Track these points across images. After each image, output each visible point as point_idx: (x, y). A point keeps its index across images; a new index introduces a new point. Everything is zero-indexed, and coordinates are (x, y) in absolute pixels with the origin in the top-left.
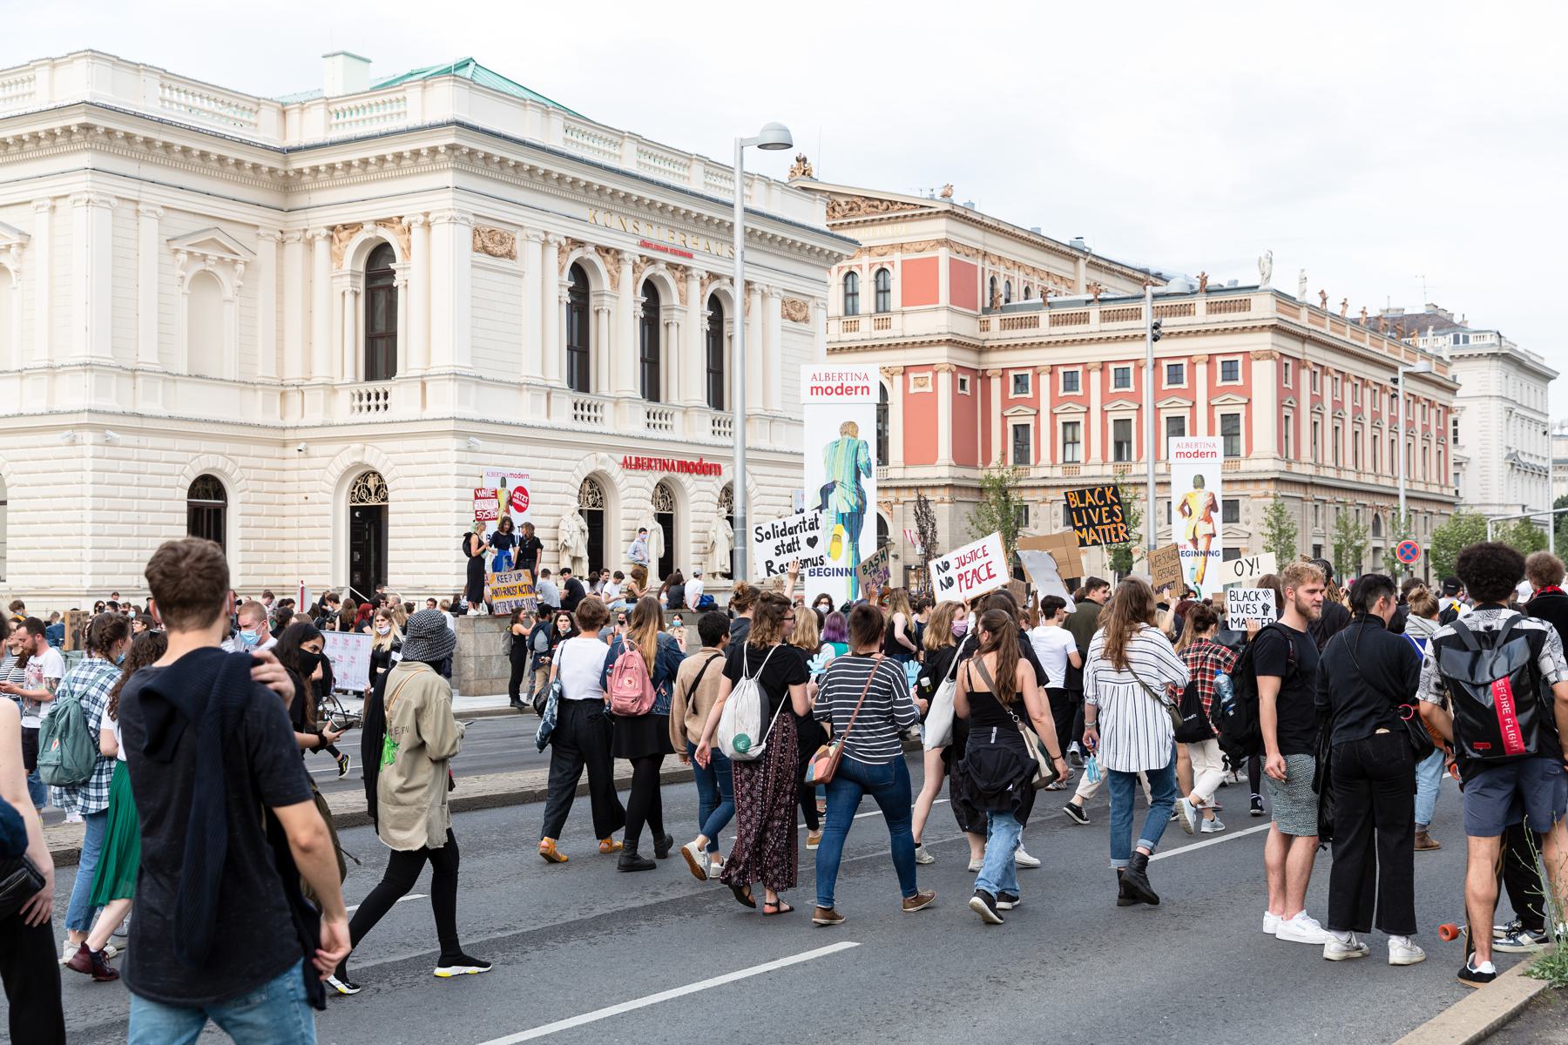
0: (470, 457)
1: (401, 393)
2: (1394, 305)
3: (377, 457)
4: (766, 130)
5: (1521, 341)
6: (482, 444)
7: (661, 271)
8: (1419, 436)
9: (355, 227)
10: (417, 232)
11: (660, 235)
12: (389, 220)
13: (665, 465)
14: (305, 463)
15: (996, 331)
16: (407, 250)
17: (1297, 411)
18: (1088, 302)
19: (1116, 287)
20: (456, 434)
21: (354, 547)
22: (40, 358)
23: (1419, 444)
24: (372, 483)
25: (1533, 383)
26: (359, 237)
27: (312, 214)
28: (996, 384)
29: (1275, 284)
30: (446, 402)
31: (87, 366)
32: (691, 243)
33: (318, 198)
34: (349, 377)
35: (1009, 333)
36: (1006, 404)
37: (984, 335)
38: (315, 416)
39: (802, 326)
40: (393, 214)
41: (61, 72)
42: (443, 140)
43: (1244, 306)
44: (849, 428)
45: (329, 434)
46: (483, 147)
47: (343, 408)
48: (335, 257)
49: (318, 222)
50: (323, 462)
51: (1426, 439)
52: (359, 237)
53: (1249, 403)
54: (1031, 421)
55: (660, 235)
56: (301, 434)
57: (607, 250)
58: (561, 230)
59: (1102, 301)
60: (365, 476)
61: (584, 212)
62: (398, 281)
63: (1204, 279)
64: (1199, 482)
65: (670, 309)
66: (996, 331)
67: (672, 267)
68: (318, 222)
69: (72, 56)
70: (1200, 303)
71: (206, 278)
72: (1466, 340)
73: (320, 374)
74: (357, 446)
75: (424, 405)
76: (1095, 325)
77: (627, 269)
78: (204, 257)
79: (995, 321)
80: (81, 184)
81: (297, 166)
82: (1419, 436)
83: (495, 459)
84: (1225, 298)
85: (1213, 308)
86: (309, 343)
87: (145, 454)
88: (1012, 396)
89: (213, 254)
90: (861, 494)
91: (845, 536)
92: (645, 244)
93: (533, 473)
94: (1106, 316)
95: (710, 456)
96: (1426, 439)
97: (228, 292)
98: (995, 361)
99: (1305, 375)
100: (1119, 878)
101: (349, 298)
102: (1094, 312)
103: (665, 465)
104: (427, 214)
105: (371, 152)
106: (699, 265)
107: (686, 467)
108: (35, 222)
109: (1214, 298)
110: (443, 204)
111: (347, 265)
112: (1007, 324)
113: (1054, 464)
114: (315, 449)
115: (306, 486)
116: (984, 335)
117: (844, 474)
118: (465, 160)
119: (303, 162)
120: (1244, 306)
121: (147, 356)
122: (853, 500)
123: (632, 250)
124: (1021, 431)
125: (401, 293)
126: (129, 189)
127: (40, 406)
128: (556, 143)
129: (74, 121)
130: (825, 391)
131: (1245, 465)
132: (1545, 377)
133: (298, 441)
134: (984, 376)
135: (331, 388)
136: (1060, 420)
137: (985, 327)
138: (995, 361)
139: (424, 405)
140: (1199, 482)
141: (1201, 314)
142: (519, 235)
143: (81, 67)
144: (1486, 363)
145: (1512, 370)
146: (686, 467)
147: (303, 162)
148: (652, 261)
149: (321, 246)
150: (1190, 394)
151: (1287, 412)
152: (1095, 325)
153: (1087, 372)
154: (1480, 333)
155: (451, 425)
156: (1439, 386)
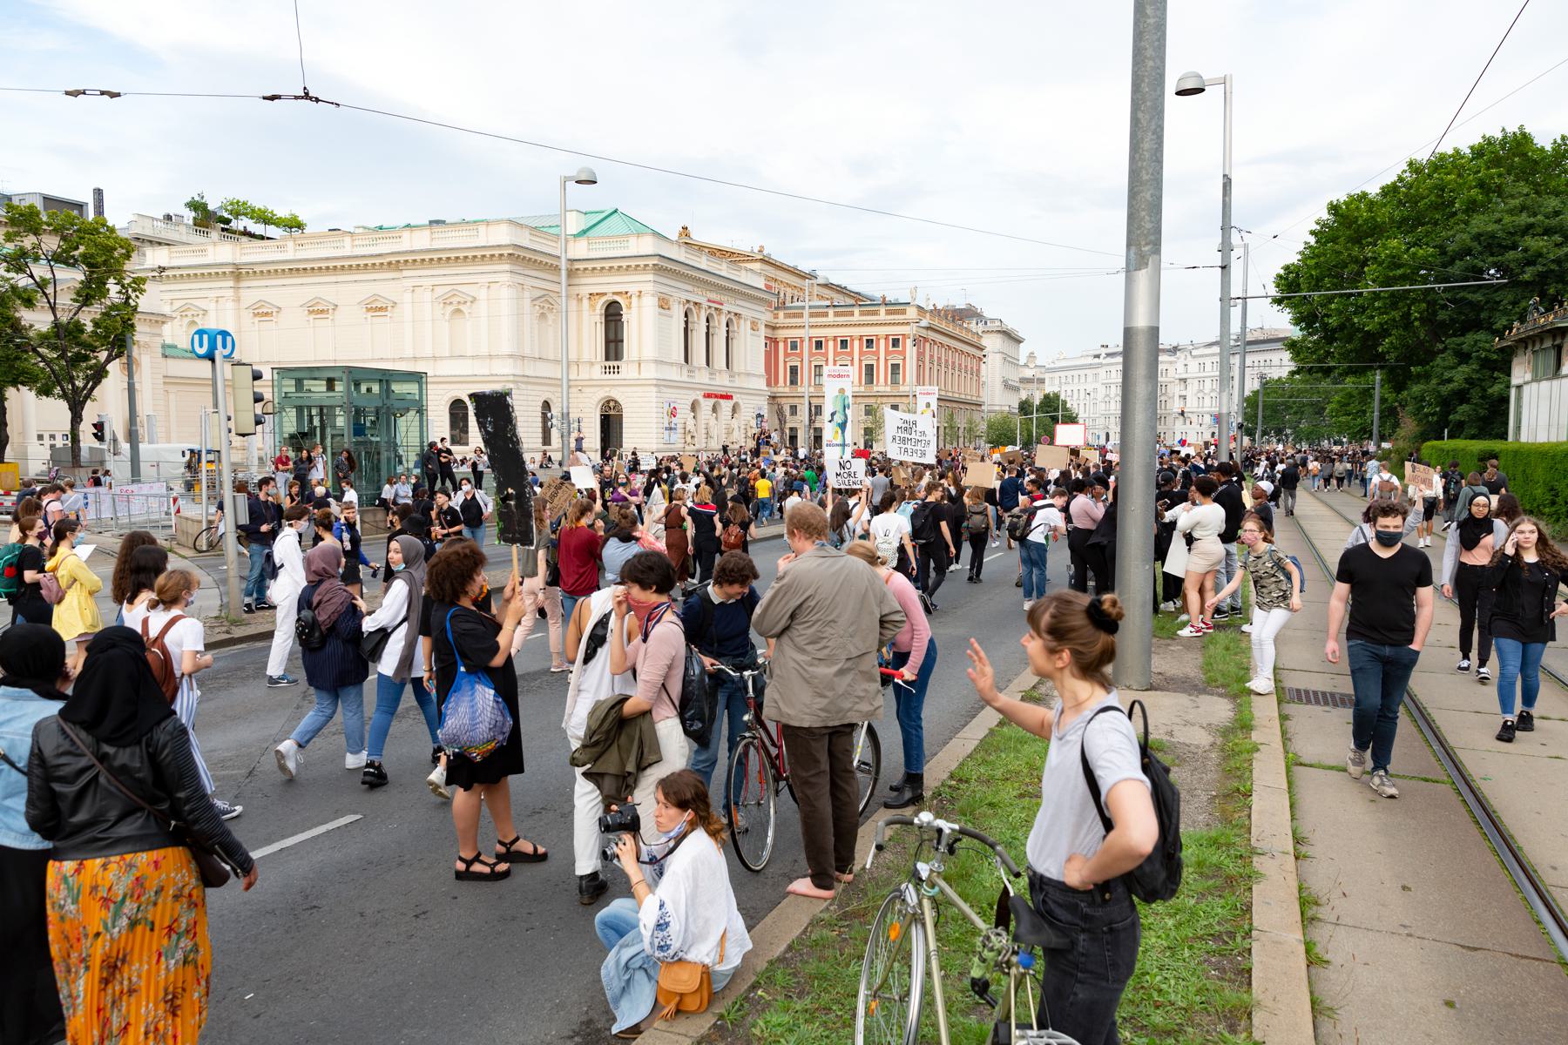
0: (659, 395)
1: (627, 369)
2: (951, 303)
3: (616, 394)
4: (581, 171)
5: (1010, 324)
6: (665, 390)
7: (732, 316)
8: (943, 365)
9: (605, 294)
10: (634, 299)
11: (713, 296)
12: (621, 293)
13: (716, 396)
14: (580, 395)
15: (782, 319)
16: (629, 307)
17: (924, 362)
18: (828, 306)
19: (839, 299)
20: (656, 385)
21: (602, 432)
22: (484, 351)
23: (969, 376)
24: (612, 404)
25: (1013, 344)
26: (604, 299)
27: (581, 288)
28: (781, 345)
29: (917, 303)
30: (650, 372)
31: (511, 356)
32: (724, 298)
33: (583, 281)
34: (599, 359)
35: (788, 320)
36: (786, 355)
37: (776, 321)
38: (584, 376)
39: (667, 312)
40: (624, 290)
41: (491, 228)
42: (651, 262)
43: (903, 312)
44: (842, 391)
45: (592, 383)
46: (670, 266)
47: (597, 372)
48: (593, 307)
49: (585, 291)
50: (590, 395)
51: (939, 365)
52: (604, 299)
53: (904, 359)
54: (798, 364)
55: (713, 296)
56: (580, 383)
57: (696, 303)
58: (685, 296)
59: (834, 306)
60: (608, 402)
61: (690, 288)
62: (624, 319)
63: (884, 298)
64: (928, 405)
65: (734, 332)
66: (782, 319)
67: (716, 309)
68: (585, 291)
69: (498, 222)
70: (882, 310)
71: (543, 315)
72: (986, 323)
73: (586, 356)
74: (608, 389)
75: (639, 373)
76: (831, 318)
77: (703, 311)
78: (543, 307)
79: (781, 314)
80: (505, 278)
81: (577, 267)
82: (943, 365)
83: (668, 395)
84: (895, 307)
85: (888, 313)
86: (579, 342)
87: (530, 393)
88: (789, 351)
89: (547, 306)
90: (846, 416)
91: (840, 431)
92: (709, 301)
93: (679, 401)
94: (836, 314)
95: (729, 391)
96: (939, 365)
97: (550, 323)
98: (781, 334)
99: (928, 345)
100: (362, 701)
101: (598, 325)
102: (831, 311)
103: (716, 396)
104: (640, 292)
105: (615, 264)
106: (725, 308)
107: (722, 397)
108: (482, 294)
109: (889, 308)
110: (649, 288)
111: (598, 311)
112: (787, 316)
113: (810, 385)
114: (584, 390)
115: (581, 405)
116: (776, 321)
117: (840, 408)
118: (658, 269)
119: (581, 266)
120: (903, 312)
121: (527, 351)
122: (843, 418)
123: (705, 304)
124: (794, 370)
125: (625, 324)
126: (520, 279)
127: (487, 372)
128: (682, 259)
129: (506, 252)
130: (834, 376)
131: (902, 388)
132: (1019, 341)
133: (577, 386)
134: (775, 341)
135: (592, 364)
136: (813, 364)
137: (776, 317)
138: (781, 334)
139: (639, 373)
140: (928, 405)
141: (882, 315)
142: (671, 299)
143: (504, 228)
144: (995, 335)
145: (1006, 338)
146: (722, 397)
147: (581, 266)
148: (710, 307)
149: (586, 302)
150: (877, 353)
151: (920, 363)
152: (831, 318)
153: (827, 341)
154: (993, 320)
155: (655, 382)
156: (978, 348)
